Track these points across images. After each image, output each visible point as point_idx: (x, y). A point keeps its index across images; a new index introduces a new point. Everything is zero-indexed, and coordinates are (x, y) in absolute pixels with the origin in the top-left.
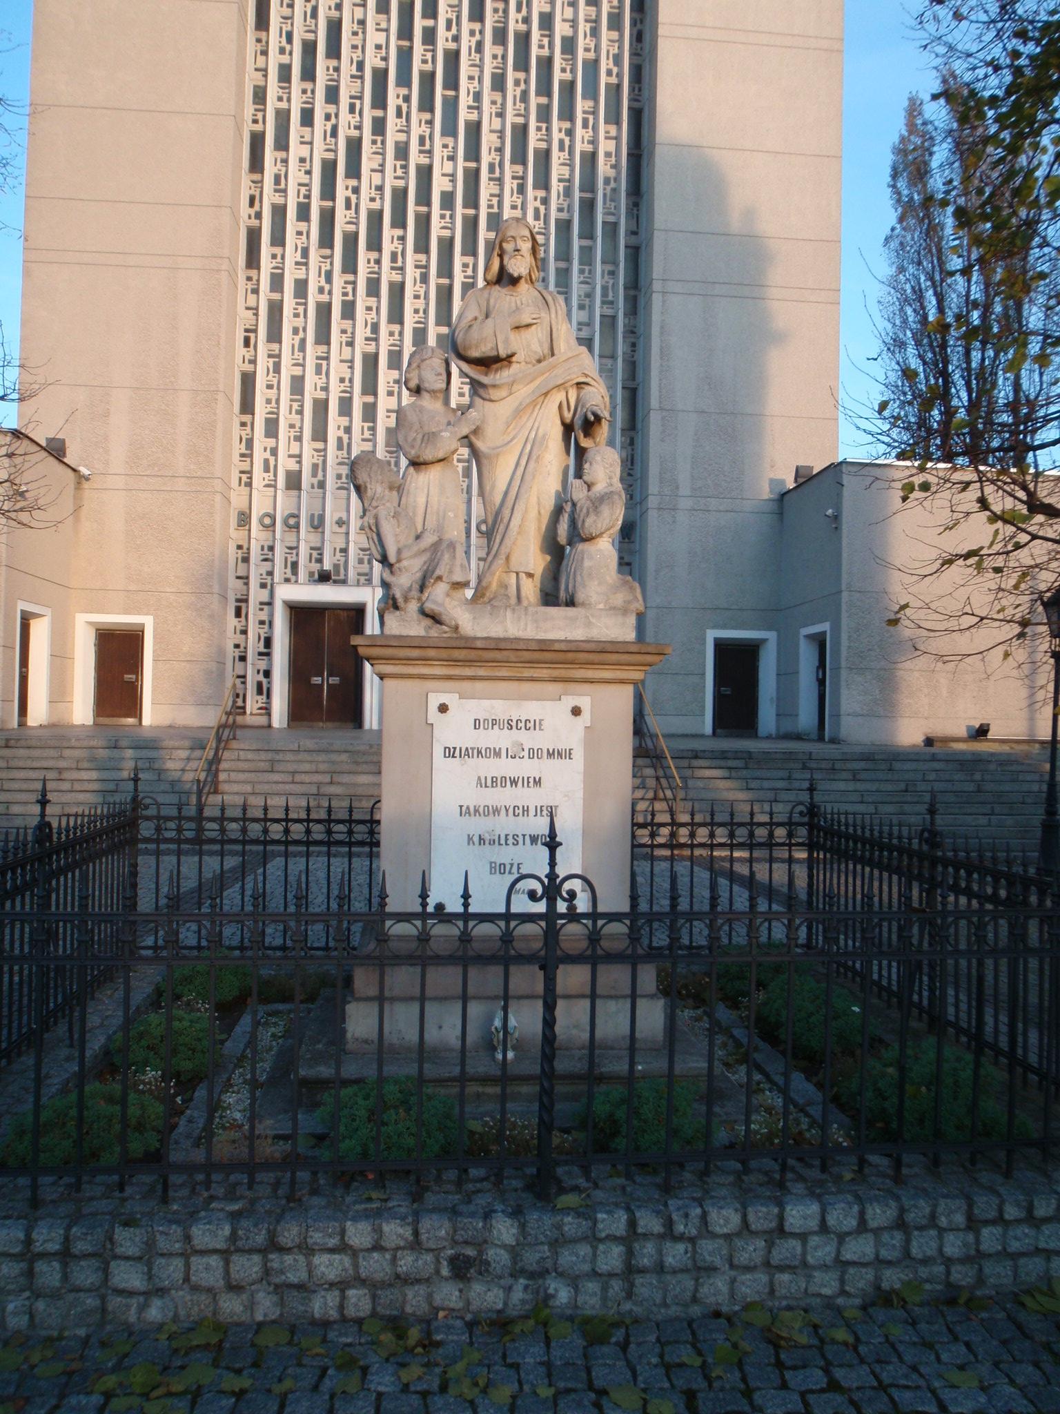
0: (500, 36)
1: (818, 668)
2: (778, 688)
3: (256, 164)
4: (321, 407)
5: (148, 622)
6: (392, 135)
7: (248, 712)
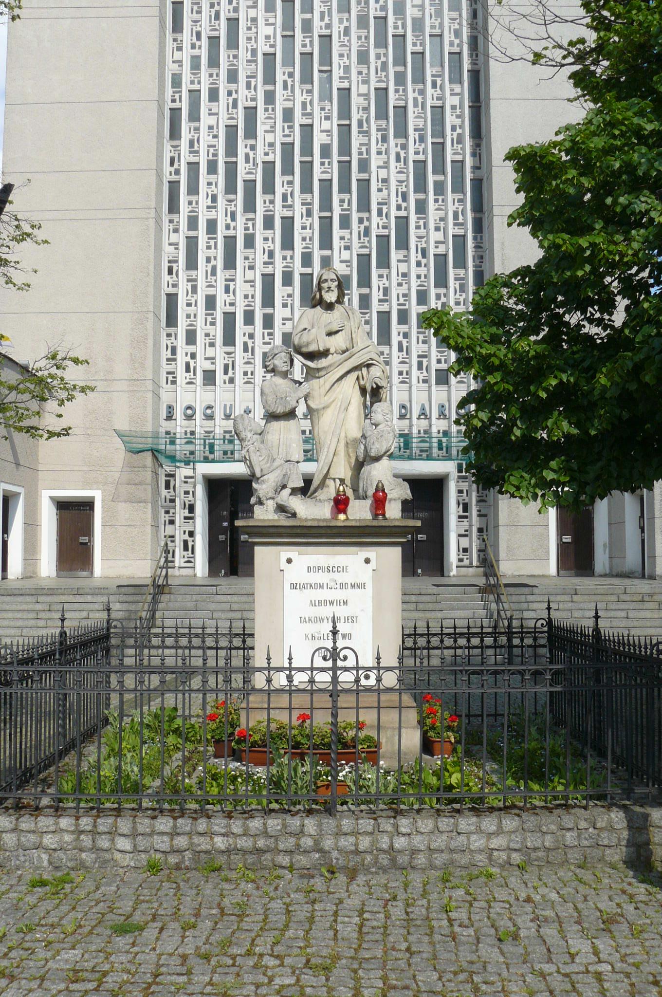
0: (363, 22)
1: (640, 517)
2: (610, 535)
3: (175, 134)
4: (229, 318)
5: (97, 496)
6: (280, 104)
7: (177, 565)
